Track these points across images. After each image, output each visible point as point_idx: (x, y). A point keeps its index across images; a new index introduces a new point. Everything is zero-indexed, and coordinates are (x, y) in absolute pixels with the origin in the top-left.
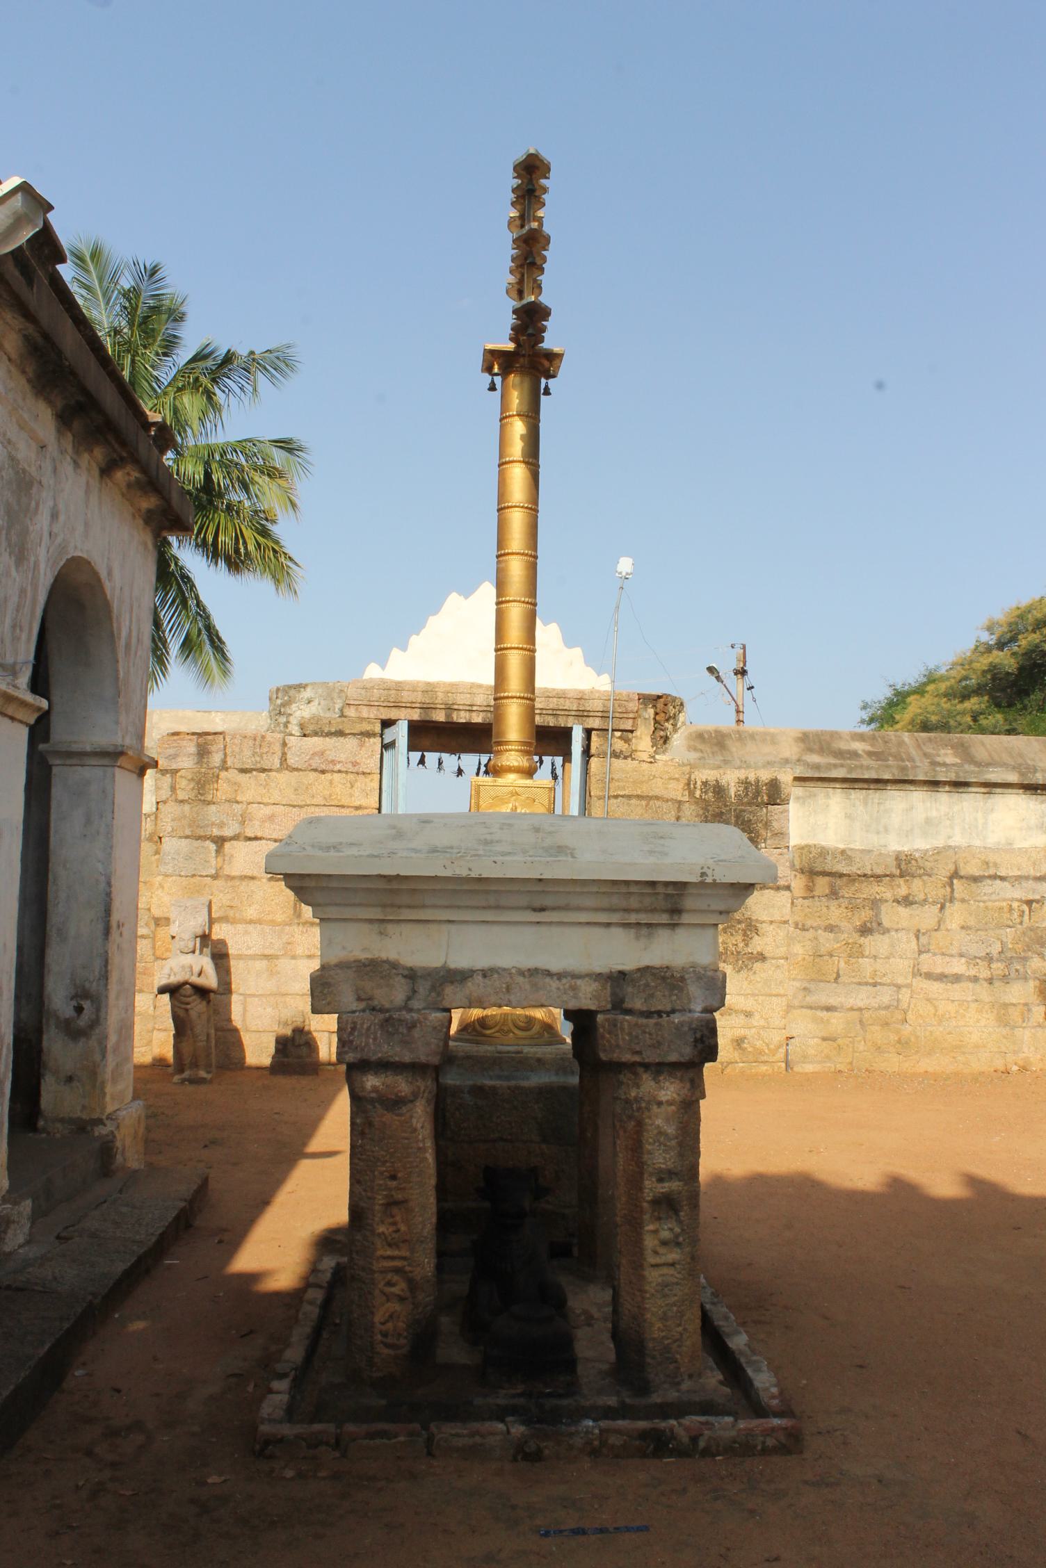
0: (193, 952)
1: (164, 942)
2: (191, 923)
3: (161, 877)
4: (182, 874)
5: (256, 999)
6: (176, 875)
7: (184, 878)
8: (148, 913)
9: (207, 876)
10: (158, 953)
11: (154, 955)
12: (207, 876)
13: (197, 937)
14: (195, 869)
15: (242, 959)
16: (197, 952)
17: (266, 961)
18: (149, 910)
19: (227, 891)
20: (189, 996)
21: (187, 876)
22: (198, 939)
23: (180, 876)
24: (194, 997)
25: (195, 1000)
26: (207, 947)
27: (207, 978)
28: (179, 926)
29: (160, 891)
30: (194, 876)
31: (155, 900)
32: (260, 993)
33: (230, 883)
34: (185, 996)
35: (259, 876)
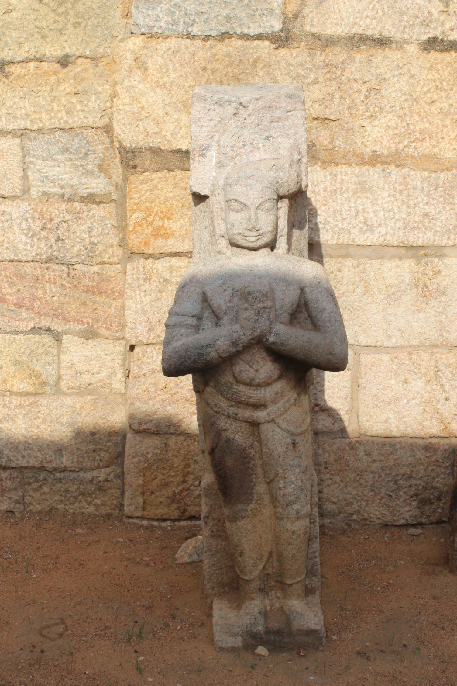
0: (272, 246)
1: (149, 212)
2: (258, 156)
3: (138, 41)
4: (195, 31)
5: (386, 357)
6: (180, 36)
7: (199, 43)
8: (104, 137)
9: (260, 37)
10: (134, 241)
11: (122, 244)
12: (260, 37)
13: (280, 198)
14: (228, 18)
15: (347, 256)
16: (282, 243)
17: (413, 262)
18: (108, 129)
19: (312, 76)
20: (267, 384)
21: (207, 38)
22: (284, 205)
23: (189, 36)
24: (278, 386)
25: (279, 395)
26: (301, 228)
27: (316, 327)
28: (220, 165)
29: (137, 75)
30: (224, 36)
31: (124, 98)
32: (393, 342)
33: (320, 58)
34: (249, 384)
35: (398, 36)
